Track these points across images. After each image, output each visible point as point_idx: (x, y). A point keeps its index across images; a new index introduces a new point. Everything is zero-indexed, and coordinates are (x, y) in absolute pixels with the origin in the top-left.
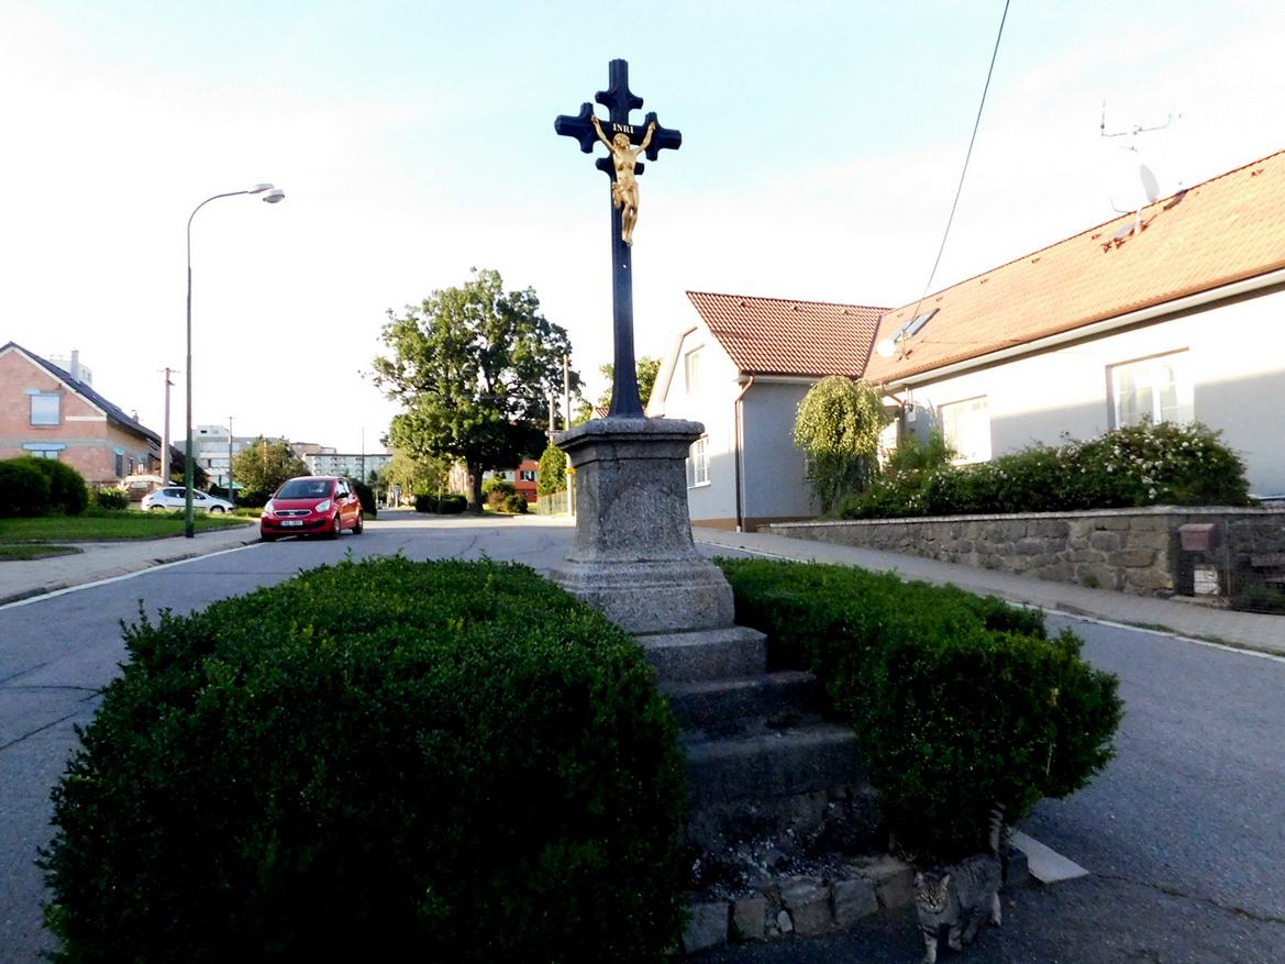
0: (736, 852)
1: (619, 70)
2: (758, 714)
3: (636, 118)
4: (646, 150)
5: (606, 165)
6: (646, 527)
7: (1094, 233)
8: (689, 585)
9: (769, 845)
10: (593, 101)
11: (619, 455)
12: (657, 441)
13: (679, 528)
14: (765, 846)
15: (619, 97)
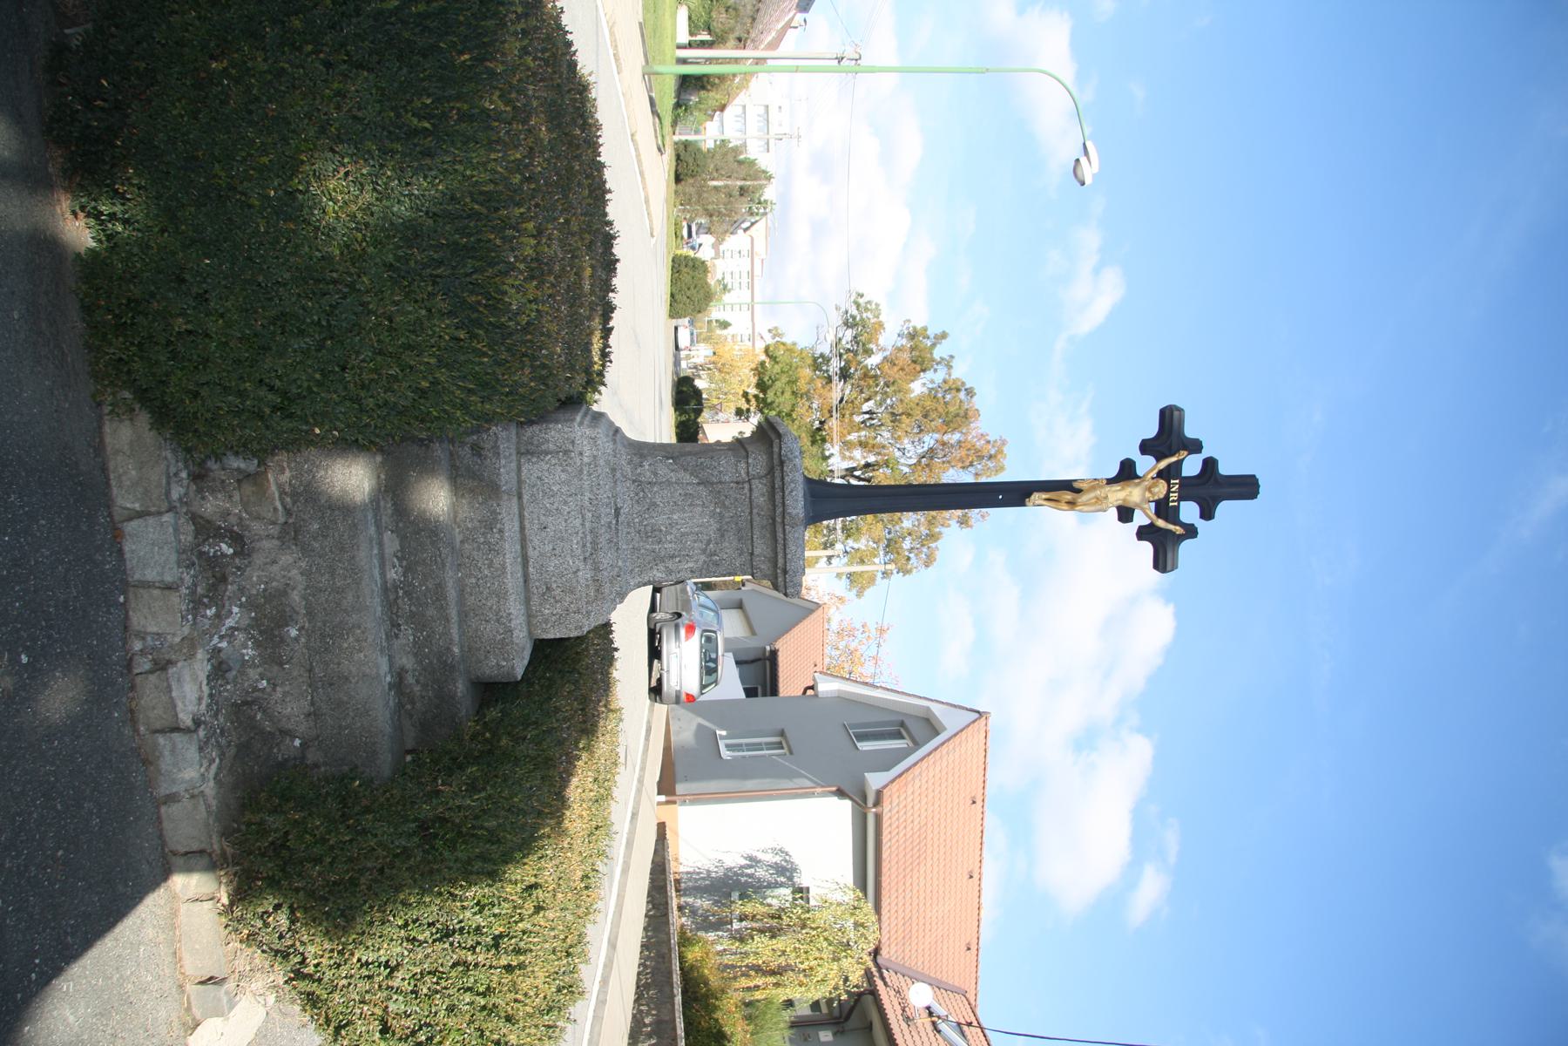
0: (240, 606)
1: (1246, 487)
2: (415, 655)
3: (1189, 512)
4: (1152, 525)
5: (1127, 472)
6: (661, 520)
7: (974, 948)
8: (585, 574)
9: (249, 653)
10: (1205, 454)
11: (755, 483)
12: (774, 533)
13: (661, 567)
14: (246, 647)
15: (1214, 488)
